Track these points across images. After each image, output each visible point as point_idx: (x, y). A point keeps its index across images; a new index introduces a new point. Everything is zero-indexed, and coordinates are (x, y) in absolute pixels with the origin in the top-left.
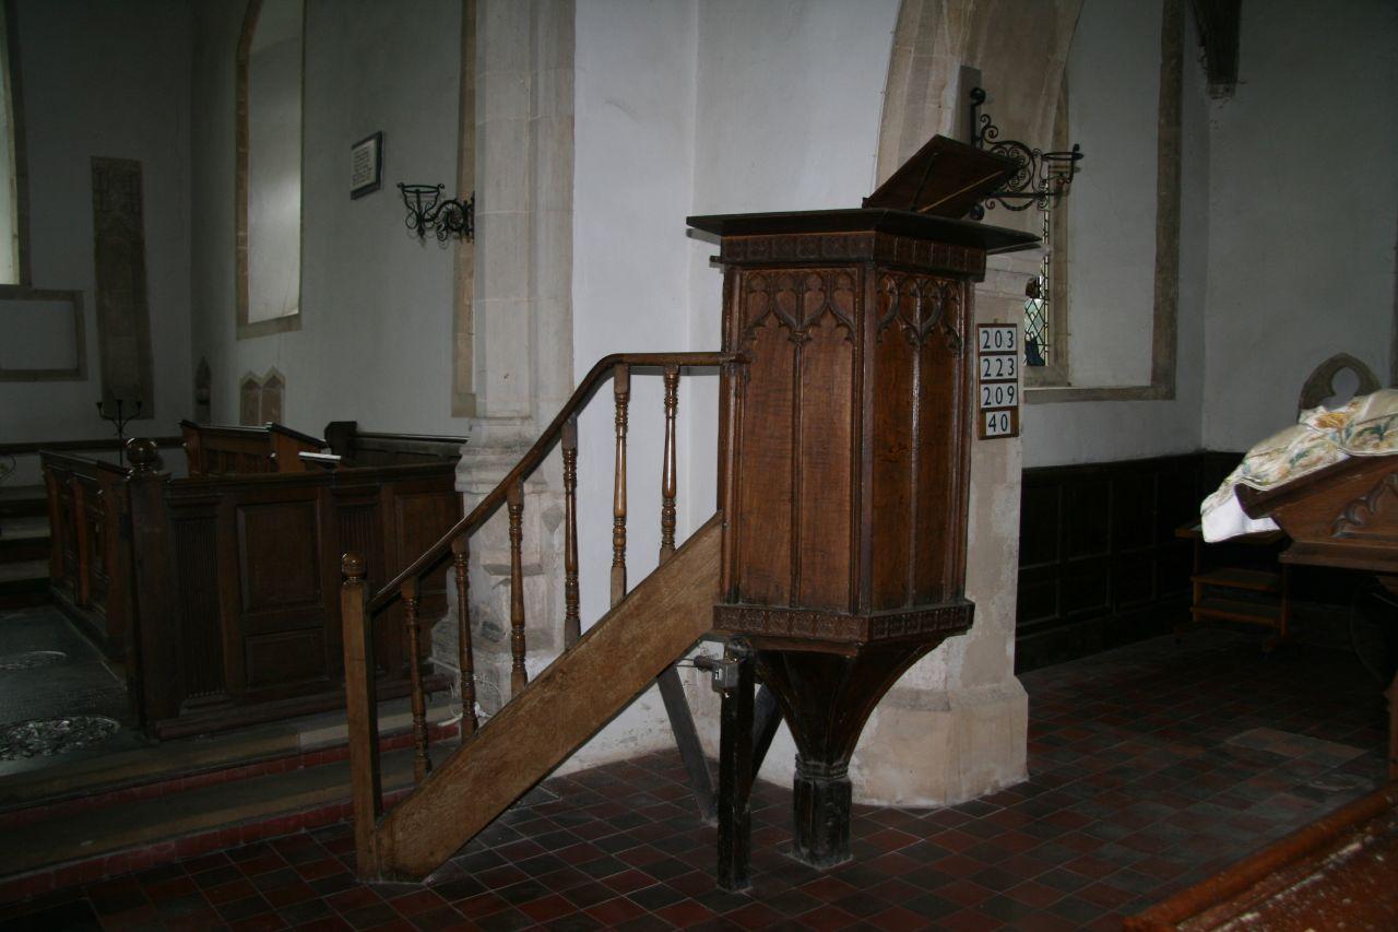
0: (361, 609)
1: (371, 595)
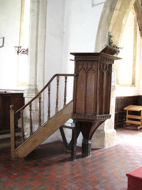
0: (13, 114)
1: (15, 112)
